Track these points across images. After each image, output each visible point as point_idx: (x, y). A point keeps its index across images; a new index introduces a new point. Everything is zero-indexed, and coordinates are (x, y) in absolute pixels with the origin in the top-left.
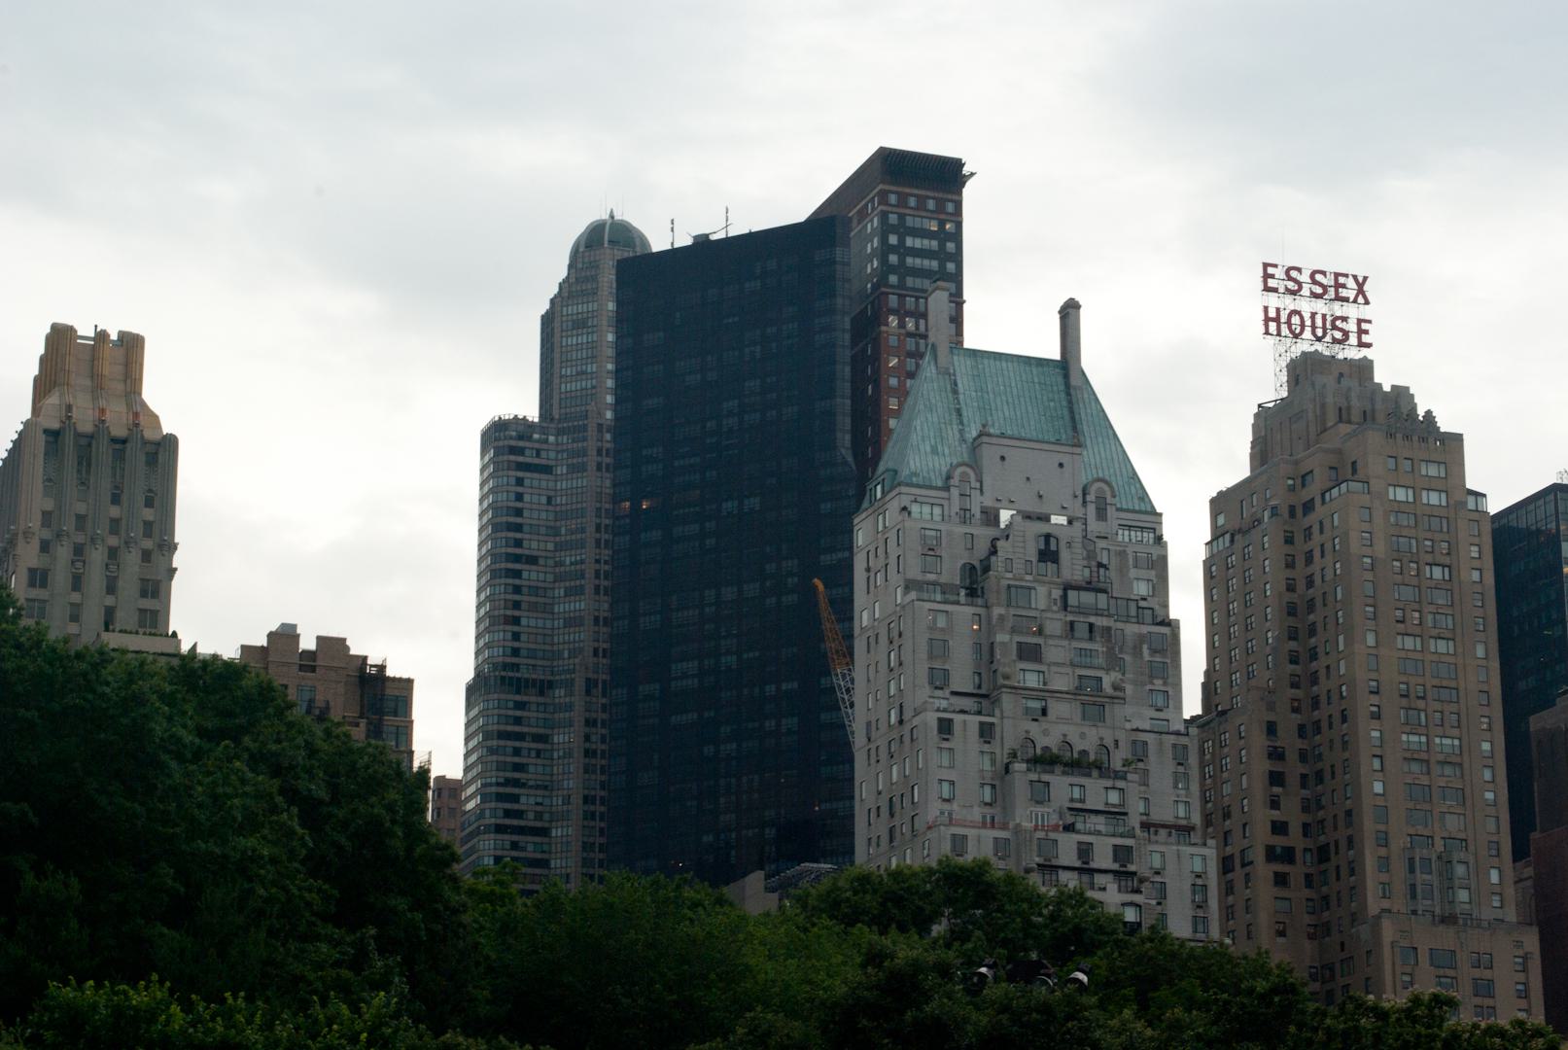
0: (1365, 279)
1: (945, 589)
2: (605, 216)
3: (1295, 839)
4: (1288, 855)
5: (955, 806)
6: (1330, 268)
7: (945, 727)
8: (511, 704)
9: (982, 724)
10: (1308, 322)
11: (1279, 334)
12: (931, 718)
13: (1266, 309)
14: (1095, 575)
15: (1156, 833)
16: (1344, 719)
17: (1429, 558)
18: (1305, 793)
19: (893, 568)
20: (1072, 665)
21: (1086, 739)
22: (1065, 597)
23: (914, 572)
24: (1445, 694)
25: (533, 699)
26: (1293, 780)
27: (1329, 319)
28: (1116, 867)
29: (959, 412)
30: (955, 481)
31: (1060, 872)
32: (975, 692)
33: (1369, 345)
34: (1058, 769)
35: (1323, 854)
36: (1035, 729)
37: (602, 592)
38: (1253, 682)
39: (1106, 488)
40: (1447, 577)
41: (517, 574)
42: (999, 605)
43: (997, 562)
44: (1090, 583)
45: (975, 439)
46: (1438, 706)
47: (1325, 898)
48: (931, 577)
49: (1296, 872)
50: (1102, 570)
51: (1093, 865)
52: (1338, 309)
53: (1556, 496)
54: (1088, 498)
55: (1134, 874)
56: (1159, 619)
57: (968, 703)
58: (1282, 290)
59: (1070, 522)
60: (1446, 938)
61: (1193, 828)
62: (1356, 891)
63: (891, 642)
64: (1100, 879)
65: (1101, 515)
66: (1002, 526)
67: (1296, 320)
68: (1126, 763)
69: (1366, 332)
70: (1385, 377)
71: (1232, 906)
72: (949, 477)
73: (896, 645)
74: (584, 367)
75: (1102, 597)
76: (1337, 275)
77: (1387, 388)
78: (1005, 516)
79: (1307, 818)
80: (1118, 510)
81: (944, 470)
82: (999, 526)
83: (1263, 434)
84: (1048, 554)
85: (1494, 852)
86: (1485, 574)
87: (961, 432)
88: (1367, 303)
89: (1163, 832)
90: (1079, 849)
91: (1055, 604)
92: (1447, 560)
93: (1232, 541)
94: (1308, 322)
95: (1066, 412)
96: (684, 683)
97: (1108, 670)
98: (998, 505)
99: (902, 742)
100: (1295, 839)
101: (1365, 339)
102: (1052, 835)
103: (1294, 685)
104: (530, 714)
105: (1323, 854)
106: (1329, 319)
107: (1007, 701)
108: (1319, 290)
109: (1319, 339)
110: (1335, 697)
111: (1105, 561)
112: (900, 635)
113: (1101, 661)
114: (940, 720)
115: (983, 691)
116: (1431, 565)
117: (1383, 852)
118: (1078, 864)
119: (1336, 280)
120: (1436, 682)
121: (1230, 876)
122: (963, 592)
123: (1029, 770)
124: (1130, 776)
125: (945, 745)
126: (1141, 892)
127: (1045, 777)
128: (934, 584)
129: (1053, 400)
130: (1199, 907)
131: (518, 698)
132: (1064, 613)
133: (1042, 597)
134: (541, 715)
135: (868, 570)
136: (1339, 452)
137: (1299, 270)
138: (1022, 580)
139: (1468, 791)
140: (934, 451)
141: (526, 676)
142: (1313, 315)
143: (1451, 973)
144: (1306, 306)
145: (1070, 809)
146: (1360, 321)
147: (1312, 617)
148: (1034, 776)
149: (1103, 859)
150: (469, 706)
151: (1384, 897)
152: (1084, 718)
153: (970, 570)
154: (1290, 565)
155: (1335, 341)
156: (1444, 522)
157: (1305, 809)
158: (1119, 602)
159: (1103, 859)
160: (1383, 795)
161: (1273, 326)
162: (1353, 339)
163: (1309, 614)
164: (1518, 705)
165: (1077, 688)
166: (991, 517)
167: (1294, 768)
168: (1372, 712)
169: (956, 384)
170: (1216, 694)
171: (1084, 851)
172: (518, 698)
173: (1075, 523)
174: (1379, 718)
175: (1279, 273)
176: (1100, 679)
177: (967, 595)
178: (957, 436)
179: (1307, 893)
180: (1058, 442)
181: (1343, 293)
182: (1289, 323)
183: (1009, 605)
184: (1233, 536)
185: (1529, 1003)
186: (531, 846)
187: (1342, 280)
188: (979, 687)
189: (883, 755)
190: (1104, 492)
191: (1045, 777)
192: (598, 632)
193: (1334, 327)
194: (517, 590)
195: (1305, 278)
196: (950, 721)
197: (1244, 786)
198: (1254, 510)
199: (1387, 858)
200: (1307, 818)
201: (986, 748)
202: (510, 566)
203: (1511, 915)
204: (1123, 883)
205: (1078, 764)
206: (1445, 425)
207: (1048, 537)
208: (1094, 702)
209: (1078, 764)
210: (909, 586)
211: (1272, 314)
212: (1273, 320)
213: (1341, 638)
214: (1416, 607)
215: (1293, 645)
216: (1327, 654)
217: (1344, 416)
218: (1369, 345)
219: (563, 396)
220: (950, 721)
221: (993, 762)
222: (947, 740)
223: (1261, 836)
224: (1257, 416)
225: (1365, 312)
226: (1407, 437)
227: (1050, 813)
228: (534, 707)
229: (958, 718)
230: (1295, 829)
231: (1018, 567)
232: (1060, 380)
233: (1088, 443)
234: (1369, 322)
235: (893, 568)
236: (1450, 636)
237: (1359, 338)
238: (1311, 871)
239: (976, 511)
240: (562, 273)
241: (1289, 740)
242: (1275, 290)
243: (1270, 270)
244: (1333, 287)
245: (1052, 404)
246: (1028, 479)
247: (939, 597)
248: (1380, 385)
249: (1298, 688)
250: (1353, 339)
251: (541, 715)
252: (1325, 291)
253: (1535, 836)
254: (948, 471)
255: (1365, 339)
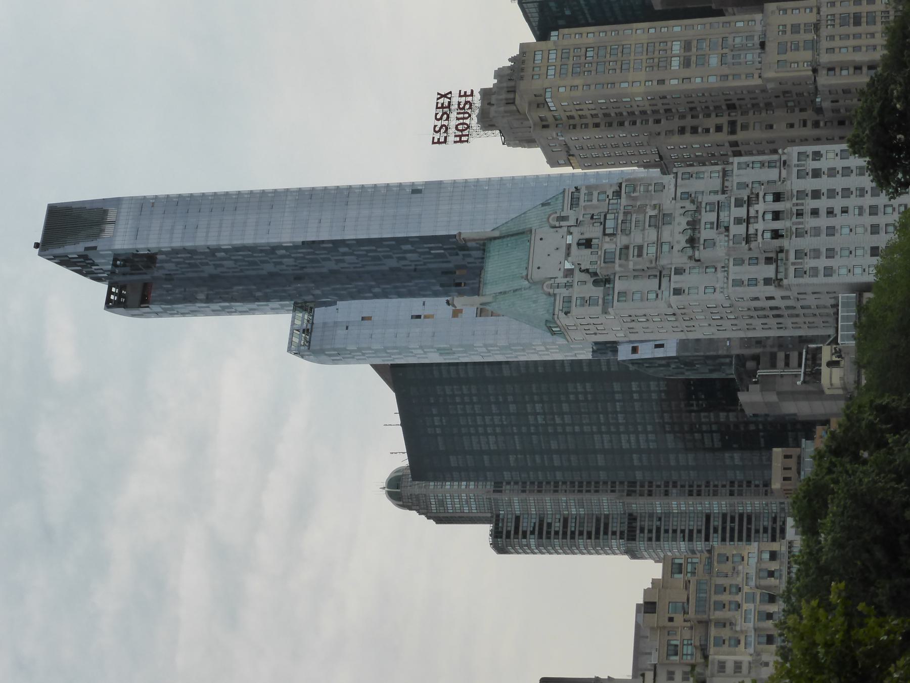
0: (438, 94)
1: (606, 294)
2: (384, 492)
3: (724, 120)
4: (733, 124)
5: (718, 286)
6: (434, 111)
7: (677, 292)
8: (642, 535)
9: (675, 274)
10: (461, 121)
11: (468, 135)
12: (674, 299)
13: (455, 142)
14: (597, 221)
15: (727, 187)
16: (665, 97)
17: (583, 58)
18: (701, 116)
19: (595, 321)
20: (644, 229)
21: (681, 222)
22: (609, 235)
23: (599, 309)
24: (650, 49)
25: (638, 524)
26: (695, 122)
27: (459, 111)
28: (745, 206)
29: (515, 291)
30: (551, 291)
31: (749, 233)
32: (658, 277)
33: (472, 91)
34: (697, 235)
35: (731, 107)
36: (677, 248)
37: (581, 489)
38: (645, 144)
39: (552, 216)
40: (592, 49)
41: (573, 533)
42: (614, 267)
43: (592, 268)
44: (601, 223)
45: (529, 282)
46: (657, 53)
47: (753, 105)
48: (600, 301)
49: (740, 120)
50: (595, 217)
51: (745, 217)
52: (454, 106)
53: (524, 3)
54: (557, 225)
55: (748, 197)
56: (618, 188)
57: (665, 281)
58: (446, 135)
59: (571, 233)
60: (771, 46)
61: (724, 169)
62: (751, 90)
63: (633, 321)
64: (752, 214)
65: (564, 218)
66: (573, 267)
67: (460, 127)
68: (693, 202)
69: (465, 92)
70: (490, 82)
71: (758, 151)
72: (549, 294)
73: (635, 318)
74: (463, 500)
75: (608, 216)
76: (437, 108)
77: (496, 81)
78: (568, 266)
79: (713, 115)
80: (563, 211)
81: (545, 297)
82: (573, 269)
83: (518, 142)
84: (587, 244)
85: (728, 25)
86: (589, 31)
87: (525, 289)
88: (450, 93)
89: (726, 184)
90: (737, 224)
91: (613, 239)
92: (583, 50)
93: (573, 155)
94: (461, 121)
95: (513, 238)
96: (632, 441)
97: (645, 213)
98: (562, 270)
99: (685, 314)
100: (724, 120)
101: (469, 93)
102: (731, 237)
103: (647, 121)
104: (646, 525)
105: (731, 107)
106: (459, 111)
107: (663, 262)
108: (445, 116)
109: (470, 116)
110: (654, 102)
111: (590, 216)
112: (630, 316)
113: (641, 217)
114: (674, 294)
115: (658, 274)
116: (586, 57)
117: (730, 78)
118: (745, 224)
119: (439, 108)
120: (645, 53)
121: (743, 152)
122: (607, 286)
123: (698, 250)
124: (700, 200)
125: (686, 291)
126: (758, 193)
127: (702, 241)
128: (604, 299)
129: (507, 244)
130: (763, 165)
131: (638, 532)
132: (617, 235)
133: (609, 245)
134: (647, 519)
135: (595, 334)
136: (530, 104)
137: (435, 126)
138: (601, 256)
139: (699, 37)
140: (535, 302)
141: (626, 527)
142: (458, 119)
143: (789, 44)
144: (453, 122)
145: (717, 229)
146: (460, 96)
147: (613, 115)
148: (702, 247)
149: (742, 212)
150: (642, 558)
151: (753, 77)
152: (670, 224)
153: (596, 283)
154: (586, 126)
155: (470, 108)
156: (564, 51)
157: (709, 116)
158: (610, 208)
159: (742, 212)
160: (702, 78)
161: (464, 138)
162: (469, 99)
163: (611, 116)
164: (649, 15)
165: (655, 228)
166: (569, 273)
167: (689, 122)
168: (831, 6)
169: (501, 293)
170: (650, 162)
171: (738, 221)
172: (638, 532)
173: (571, 231)
174: (834, 2)
175: (437, 136)
176: (650, 216)
177: (609, 284)
178: (527, 291)
179: (751, 113)
180: (529, 241)
181: (446, 104)
182: (462, 131)
183: (614, 262)
184: (570, 155)
185: (802, 7)
186: (716, 522)
187: (440, 105)
188: (656, 276)
189: (691, 323)
190: (553, 218)
191: (702, 241)
192: (602, 490)
193: (463, 108)
194: (581, 533)
195: (439, 123)
196: (674, 289)
197: (698, 146)
198: (557, 145)
199: (733, 75)
200: (713, 115)
201: (687, 271)
202: (569, 536)
203: (758, 17)
204: (754, 202)
205: (694, 225)
206: (516, 52)
207: (579, 244)
208: (661, 219)
209: (694, 225)
210: (605, 312)
211: (458, 139)
212: (460, 139)
213: (624, 100)
214: (607, 64)
215: (626, 123)
216: (631, 106)
217: (511, 101)
218: (472, 91)
219: (478, 511)
220: (674, 289)
221: (694, 268)
222: (684, 290)
223: (724, 137)
224: (509, 145)
225: (455, 94)
226: (522, 70)
227: (721, 240)
228: (643, 523)
229: (673, 286)
230: (719, 121)
231: (594, 258)
232: (497, 241)
233: (530, 226)
234: (460, 91)
235: (595, 321)
236: (621, 47)
237: (446, 108)
238: (739, 113)
239: (565, 280)
240: (414, 513)
241: (676, 123)
242: (446, 138)
243: (436, 140)
244: (444, 109)
245: (509, 245)
246: (549, 255)
247: (611, 297)
248: (494, 85)
249: (648, 120)
250: (469, 99)
251: (647, 519)
252: (446, 113)
253: (714, 6)
254: (546, 295)
255: (469, 93)
